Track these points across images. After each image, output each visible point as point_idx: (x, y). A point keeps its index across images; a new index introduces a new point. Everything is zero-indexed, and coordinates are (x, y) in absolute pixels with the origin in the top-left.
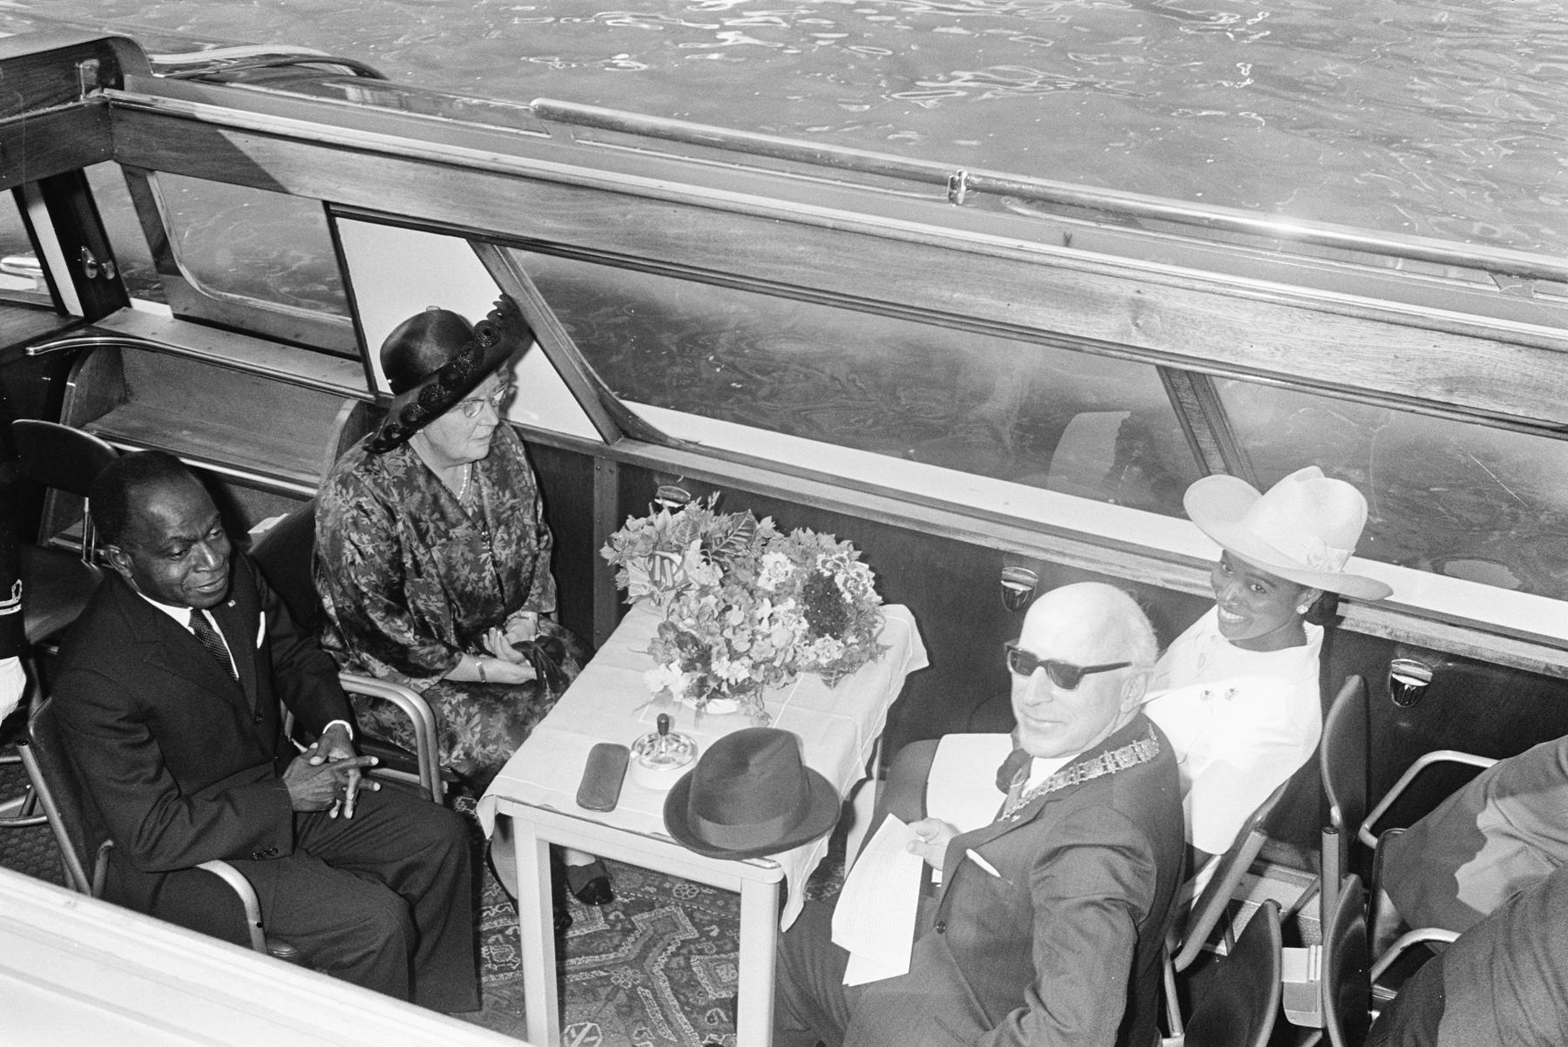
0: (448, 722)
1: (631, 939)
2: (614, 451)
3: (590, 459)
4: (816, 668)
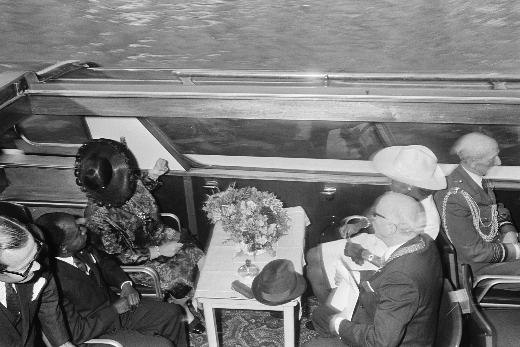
1: (228, 330)
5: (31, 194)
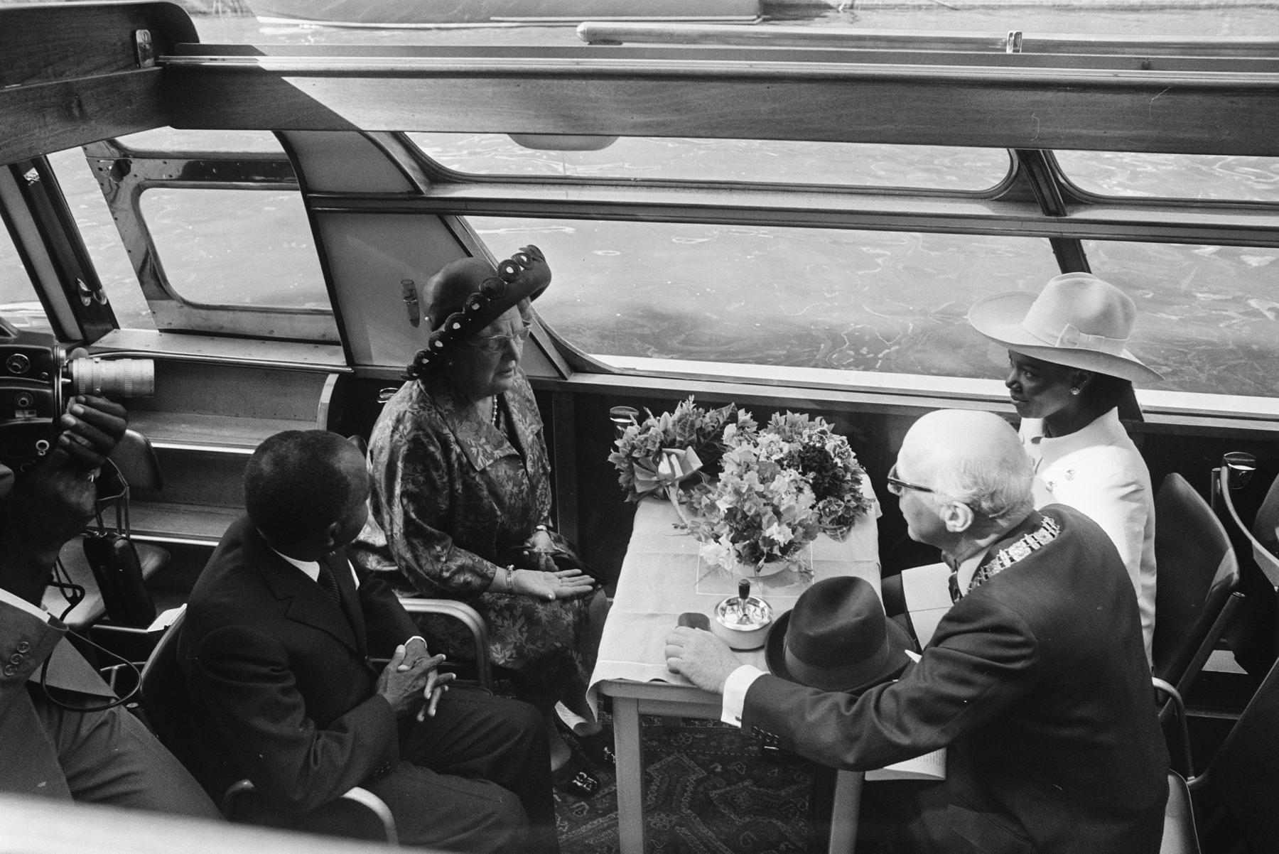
0: (497, 626)
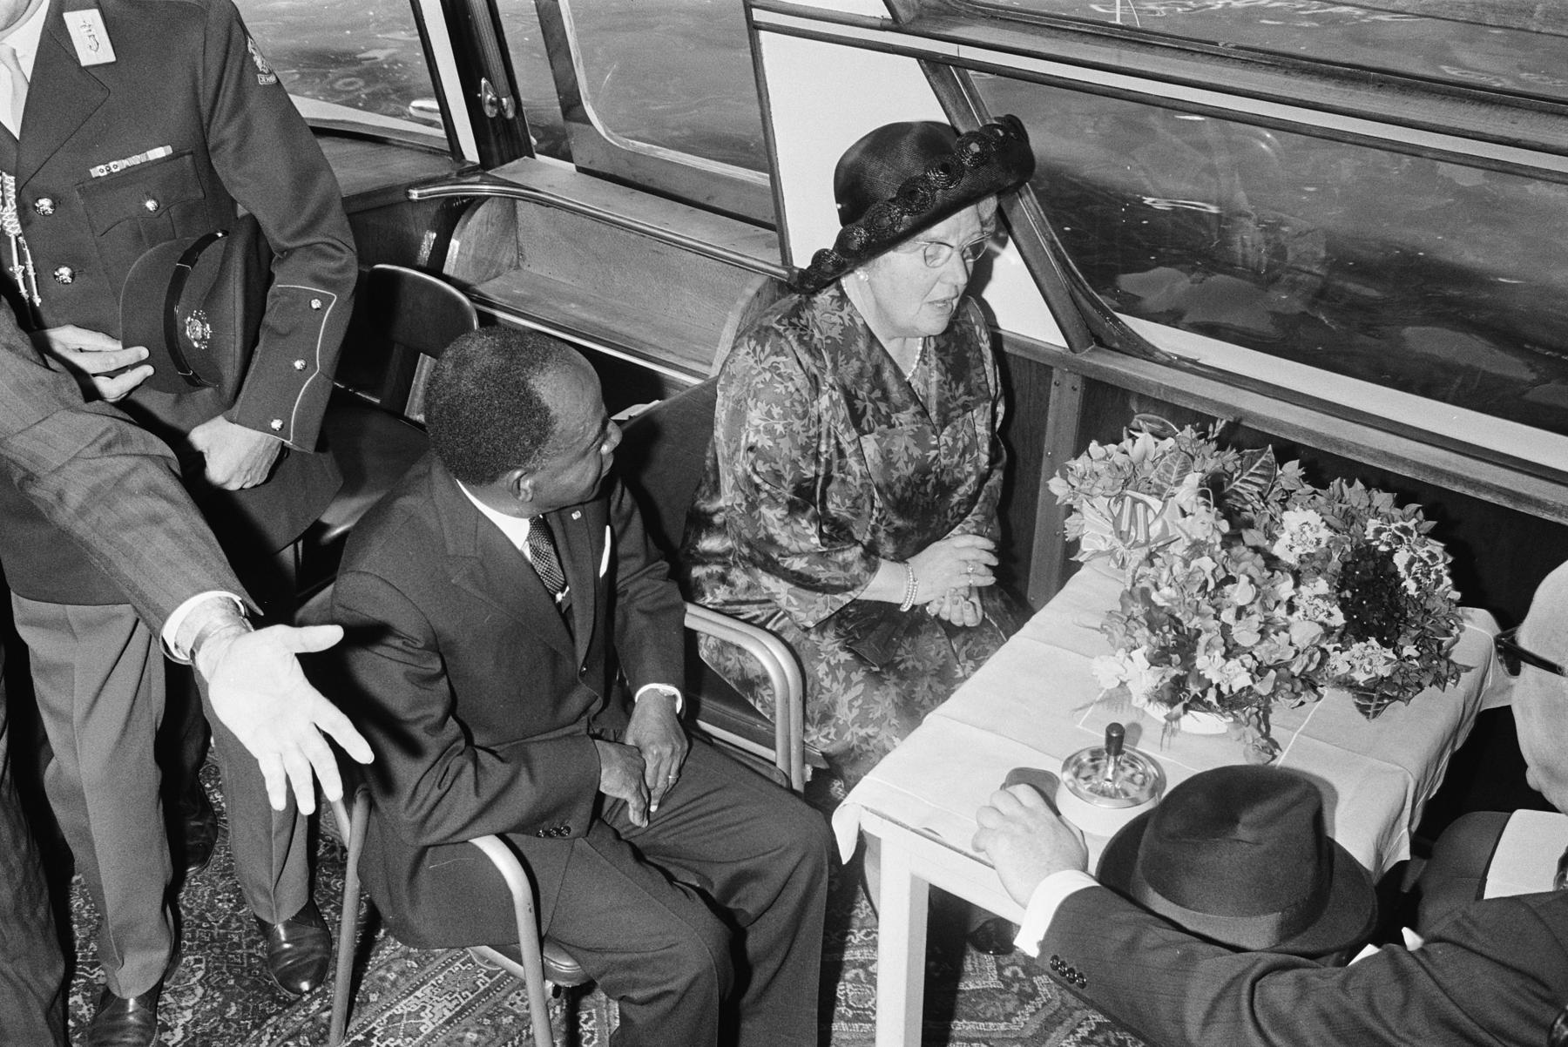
0: (822, 687)
1: (1030, 1008)
2: (1079, 362)
3: (1047, 370)
4: (1347, 684)
5: (562, 307)
